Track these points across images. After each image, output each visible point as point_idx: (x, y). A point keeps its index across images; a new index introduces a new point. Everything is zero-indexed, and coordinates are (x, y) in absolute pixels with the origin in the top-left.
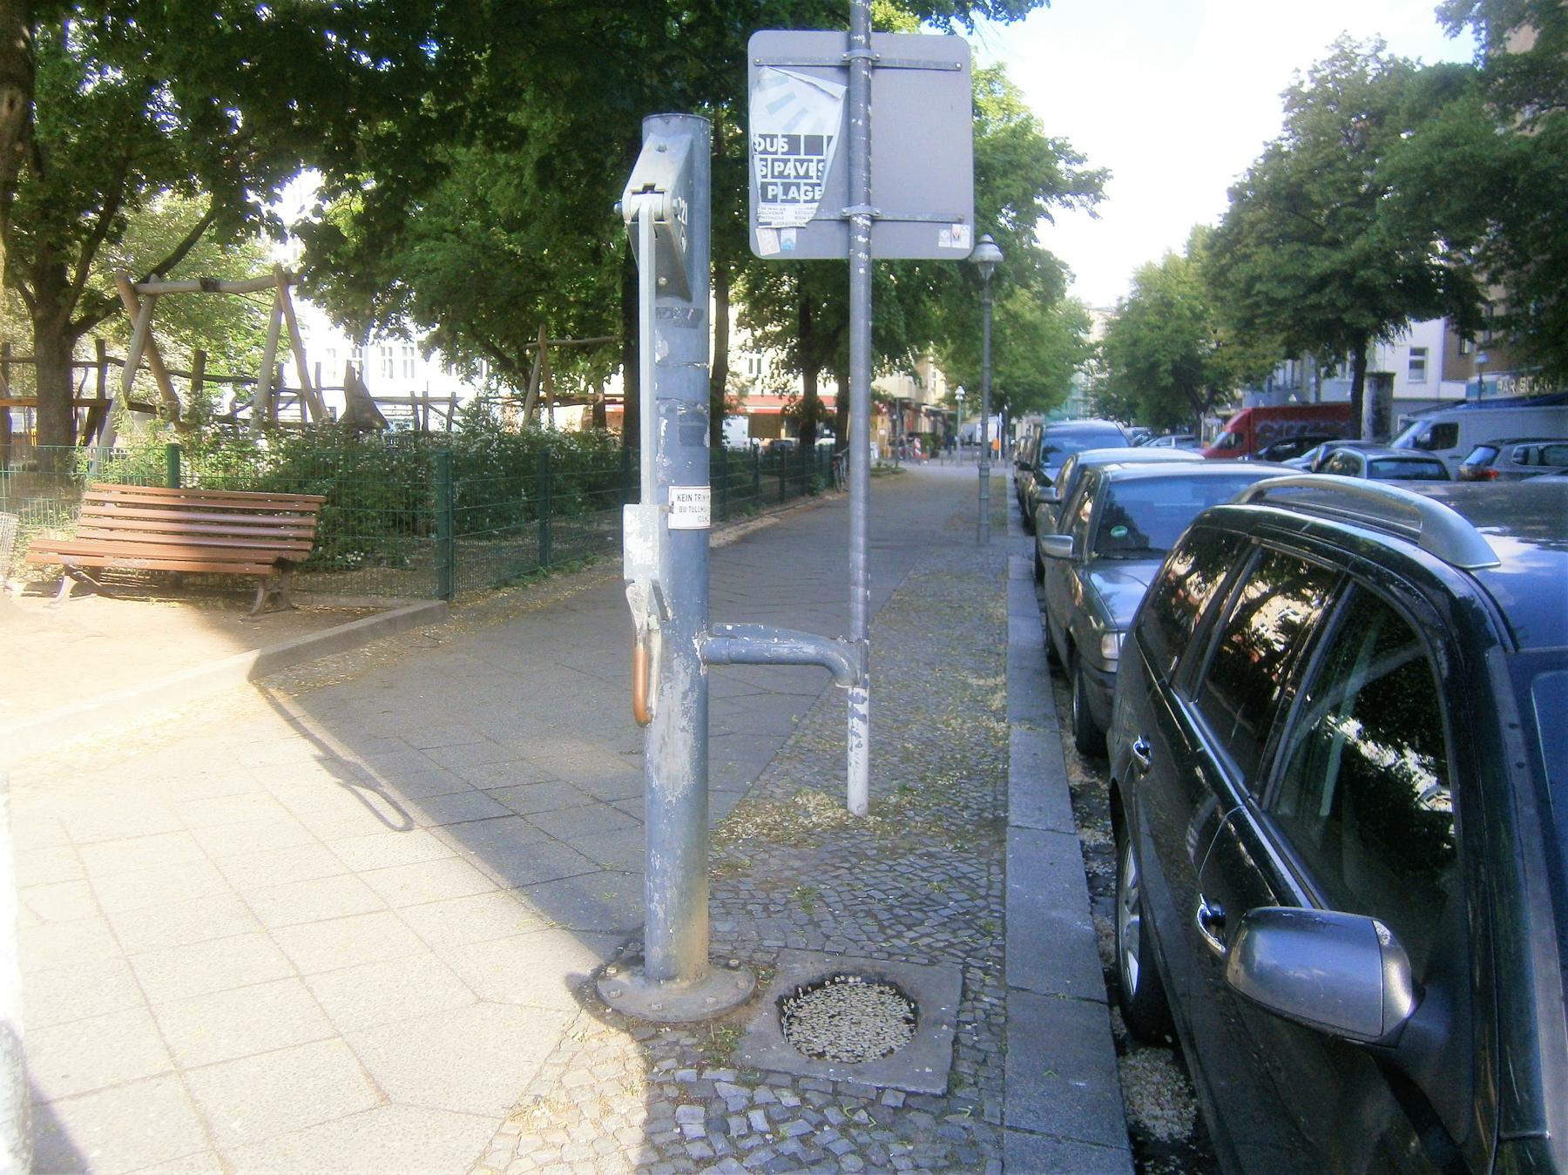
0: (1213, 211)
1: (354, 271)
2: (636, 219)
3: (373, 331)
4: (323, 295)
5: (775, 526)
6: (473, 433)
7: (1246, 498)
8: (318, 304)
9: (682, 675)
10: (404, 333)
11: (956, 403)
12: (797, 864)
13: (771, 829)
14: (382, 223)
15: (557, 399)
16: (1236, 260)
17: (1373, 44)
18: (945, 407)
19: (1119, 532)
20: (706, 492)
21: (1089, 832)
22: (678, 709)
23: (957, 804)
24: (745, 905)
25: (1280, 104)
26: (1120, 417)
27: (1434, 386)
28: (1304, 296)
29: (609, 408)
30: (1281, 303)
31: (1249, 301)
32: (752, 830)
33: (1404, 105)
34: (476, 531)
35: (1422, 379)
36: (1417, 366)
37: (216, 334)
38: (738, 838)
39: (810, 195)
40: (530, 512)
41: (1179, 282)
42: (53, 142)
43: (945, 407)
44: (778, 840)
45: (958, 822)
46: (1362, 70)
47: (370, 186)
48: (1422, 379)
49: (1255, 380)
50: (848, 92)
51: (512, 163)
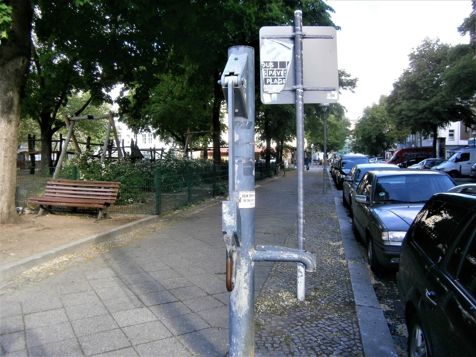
0: (388, 91)
1: (134, 113)
2: (227, 86)
3: (140, 130)
4: (125, 120)
5: (259, 187)
6: (169, 160)
7: (459, 191)
8: (124, 122)
9: (244, 266)
10: (149, 130)
11: (311, 149)
12: (282, 323)
13: (271, 308)
14: (141, 98)
15: (193, 149)
16: (396, 105)
17: (436, 40)
18: (308, 150)
19: (382, 194)
20: (254, 193)
21: (383, 305)
22: (243, 280)
23: (336, 295)
24: (264, 344)
25: (408, 58)
26: (360, 152)
27: (457, 141)
28: (417, 115)
29: (208, 152)
30: (411, 117)
31: (401, 117)
32: (264, 308)
33: (448, 58)
34: (168, 190)
35: (453, 139)
36: (451, 135)
37: (96, 132)
38: (259, 311)
39: (282, 82)
40: (185, 185)
41: (377, 112)
42: (46, 76)
43: (308, 150)
44: (274, 312)
45: (337, 303)
46: (433, 48)
47: (137, 86)
48: (453, 139)
49: (401, 141)
50: (294, 47)
51: (180, 80)
